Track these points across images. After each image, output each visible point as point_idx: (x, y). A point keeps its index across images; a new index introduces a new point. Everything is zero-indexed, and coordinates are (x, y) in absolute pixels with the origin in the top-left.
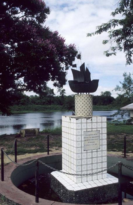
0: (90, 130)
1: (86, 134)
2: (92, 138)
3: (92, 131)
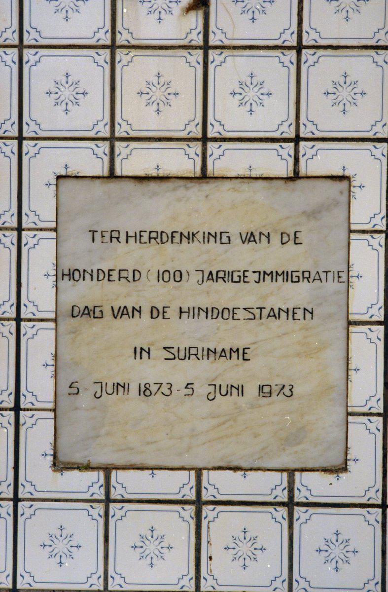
0: (180, 161)
1: (107, 225)
2: (194, 294)
3: (204, 176)
